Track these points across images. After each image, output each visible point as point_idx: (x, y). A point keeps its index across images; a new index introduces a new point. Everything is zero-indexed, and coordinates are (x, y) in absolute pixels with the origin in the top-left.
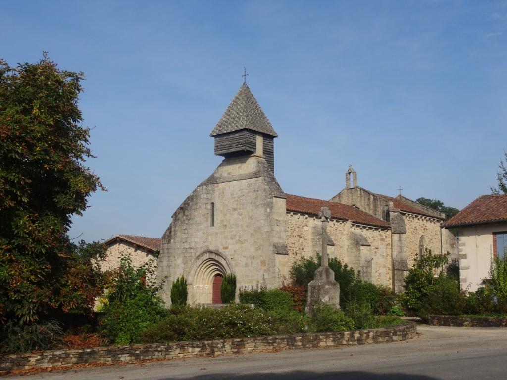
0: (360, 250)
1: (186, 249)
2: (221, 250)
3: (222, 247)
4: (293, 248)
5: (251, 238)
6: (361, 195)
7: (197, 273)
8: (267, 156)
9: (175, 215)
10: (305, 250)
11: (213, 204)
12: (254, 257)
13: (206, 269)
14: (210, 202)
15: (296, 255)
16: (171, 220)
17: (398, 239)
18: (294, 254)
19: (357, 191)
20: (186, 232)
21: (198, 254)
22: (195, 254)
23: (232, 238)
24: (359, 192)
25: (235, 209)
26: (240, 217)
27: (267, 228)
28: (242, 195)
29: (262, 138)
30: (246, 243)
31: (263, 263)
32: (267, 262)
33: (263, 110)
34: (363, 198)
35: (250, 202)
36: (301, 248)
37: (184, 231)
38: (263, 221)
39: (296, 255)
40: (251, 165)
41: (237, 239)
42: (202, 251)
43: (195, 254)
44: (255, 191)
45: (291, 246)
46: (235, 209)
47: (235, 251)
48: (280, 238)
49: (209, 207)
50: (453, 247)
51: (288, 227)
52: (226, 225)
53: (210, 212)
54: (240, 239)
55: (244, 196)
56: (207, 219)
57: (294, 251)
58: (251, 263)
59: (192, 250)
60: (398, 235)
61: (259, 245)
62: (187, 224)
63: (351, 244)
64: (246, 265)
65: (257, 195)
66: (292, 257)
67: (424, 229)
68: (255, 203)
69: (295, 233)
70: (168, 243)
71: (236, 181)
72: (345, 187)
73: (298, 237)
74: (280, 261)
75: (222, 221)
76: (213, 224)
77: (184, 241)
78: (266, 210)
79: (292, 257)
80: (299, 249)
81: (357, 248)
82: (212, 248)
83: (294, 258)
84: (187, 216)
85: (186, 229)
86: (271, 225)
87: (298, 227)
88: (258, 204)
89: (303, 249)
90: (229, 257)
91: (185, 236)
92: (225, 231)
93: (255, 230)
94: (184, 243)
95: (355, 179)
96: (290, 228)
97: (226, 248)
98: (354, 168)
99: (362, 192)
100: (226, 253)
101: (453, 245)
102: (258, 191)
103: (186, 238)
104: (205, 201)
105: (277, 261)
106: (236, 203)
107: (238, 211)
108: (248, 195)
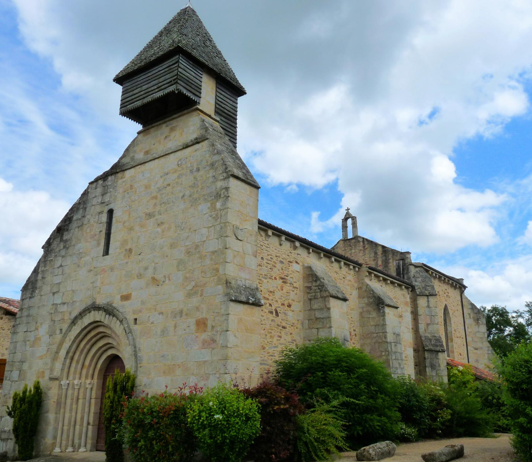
0: (384, 314)
1: (57, 304)
2: (117, 303)
3: (119, 296)
4: (271, 302)
5: (179, 270)
6: (364, 247)
7: (71, 354)
8: (224, 119)
9: (48, 246)
10: (292, 308)
11: (111, 212)
12: (181, 312)
13: (88, 347)
14: (106, 209)
15: (277, 314)
16: (41, 252)
17: (427, 305)
18: (271, 312)
19: (359, 242)
20: (60, 273)
21: (75, 313)
22: (70, 314)
23: (140, 276)
24: (362, 243)
25: (150, 215)
26: (159, 230)
27: (214, 245)
28: (166, 183)
29: (215, 82)
30: (167, 281)
31: (201, 324)
32: (210, 323)
33: (220, 49)
34: (367, 251)
35: (181, 195)
36: (286, 303)
37: (56, 271)
38: (204, 231)
39: (277, 314)
40: (189, 126)
41: (149, 273)
42: (83, 307)
43: (70, 314)
44: (191, 171)
45: (267, 296)
46: (150, 215)
47: (143, 303)
48: (242, 267)
49: (104, 218)
50: (478, 323)
51: (262, 258)
52: (130, 250)
53: (104, 228)
54: (156, 276)
55: (169, 185)
56: (99, 244)
57: (273, 308)
58: (175, 327)
59: (66, 306)
60: (426, 298)
61: (193, 283)
62: (63, 257)
63: (368, 304)
64: (164, 332)
65: (195, 178)
66: (268, 318)
67: (447, 296)
68: (190, 196)
69: (276, 273)
70: (30, 298)
71: (156, 160)
72: (341, 238)
73: (280, 282)
74: (240, 320)
75: (125, 242)
76: (106, 252)
77: (55, 291)
78: (213, 207)
79: (268, 318)
80: (283, 304)
81: (380, 310)
82: (101, 301)
83: (272, 320)
84: (66, 241)
85: (61, 266)
86: (222, 236)
87: (282, 262)
88: (196, 196)
89: (289, 306)
90: (131, 318)
91: (57, 280)
92: (127, 263)
93: (188, 253)
94: (54, 294)
95: (354, 225)
96: (265, 261)
97: (126, 298)
98: (352, 212)
99: (366, 243)
100: (128, 309)
101: (478, 320)
102: (198, 170)
103: (59, 284)
104: (98, 209)
105: (232, 318)
106: (154, 201)
107: (157, 217)
108: (177, 183)
